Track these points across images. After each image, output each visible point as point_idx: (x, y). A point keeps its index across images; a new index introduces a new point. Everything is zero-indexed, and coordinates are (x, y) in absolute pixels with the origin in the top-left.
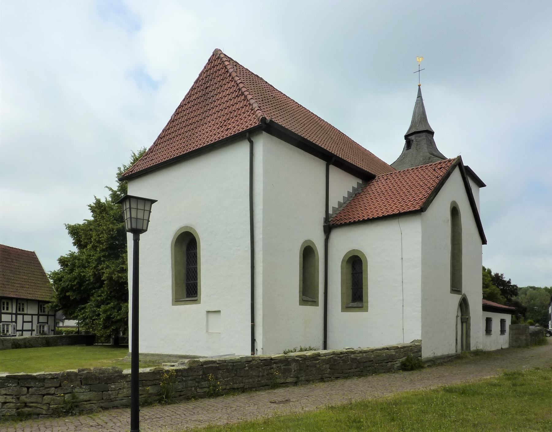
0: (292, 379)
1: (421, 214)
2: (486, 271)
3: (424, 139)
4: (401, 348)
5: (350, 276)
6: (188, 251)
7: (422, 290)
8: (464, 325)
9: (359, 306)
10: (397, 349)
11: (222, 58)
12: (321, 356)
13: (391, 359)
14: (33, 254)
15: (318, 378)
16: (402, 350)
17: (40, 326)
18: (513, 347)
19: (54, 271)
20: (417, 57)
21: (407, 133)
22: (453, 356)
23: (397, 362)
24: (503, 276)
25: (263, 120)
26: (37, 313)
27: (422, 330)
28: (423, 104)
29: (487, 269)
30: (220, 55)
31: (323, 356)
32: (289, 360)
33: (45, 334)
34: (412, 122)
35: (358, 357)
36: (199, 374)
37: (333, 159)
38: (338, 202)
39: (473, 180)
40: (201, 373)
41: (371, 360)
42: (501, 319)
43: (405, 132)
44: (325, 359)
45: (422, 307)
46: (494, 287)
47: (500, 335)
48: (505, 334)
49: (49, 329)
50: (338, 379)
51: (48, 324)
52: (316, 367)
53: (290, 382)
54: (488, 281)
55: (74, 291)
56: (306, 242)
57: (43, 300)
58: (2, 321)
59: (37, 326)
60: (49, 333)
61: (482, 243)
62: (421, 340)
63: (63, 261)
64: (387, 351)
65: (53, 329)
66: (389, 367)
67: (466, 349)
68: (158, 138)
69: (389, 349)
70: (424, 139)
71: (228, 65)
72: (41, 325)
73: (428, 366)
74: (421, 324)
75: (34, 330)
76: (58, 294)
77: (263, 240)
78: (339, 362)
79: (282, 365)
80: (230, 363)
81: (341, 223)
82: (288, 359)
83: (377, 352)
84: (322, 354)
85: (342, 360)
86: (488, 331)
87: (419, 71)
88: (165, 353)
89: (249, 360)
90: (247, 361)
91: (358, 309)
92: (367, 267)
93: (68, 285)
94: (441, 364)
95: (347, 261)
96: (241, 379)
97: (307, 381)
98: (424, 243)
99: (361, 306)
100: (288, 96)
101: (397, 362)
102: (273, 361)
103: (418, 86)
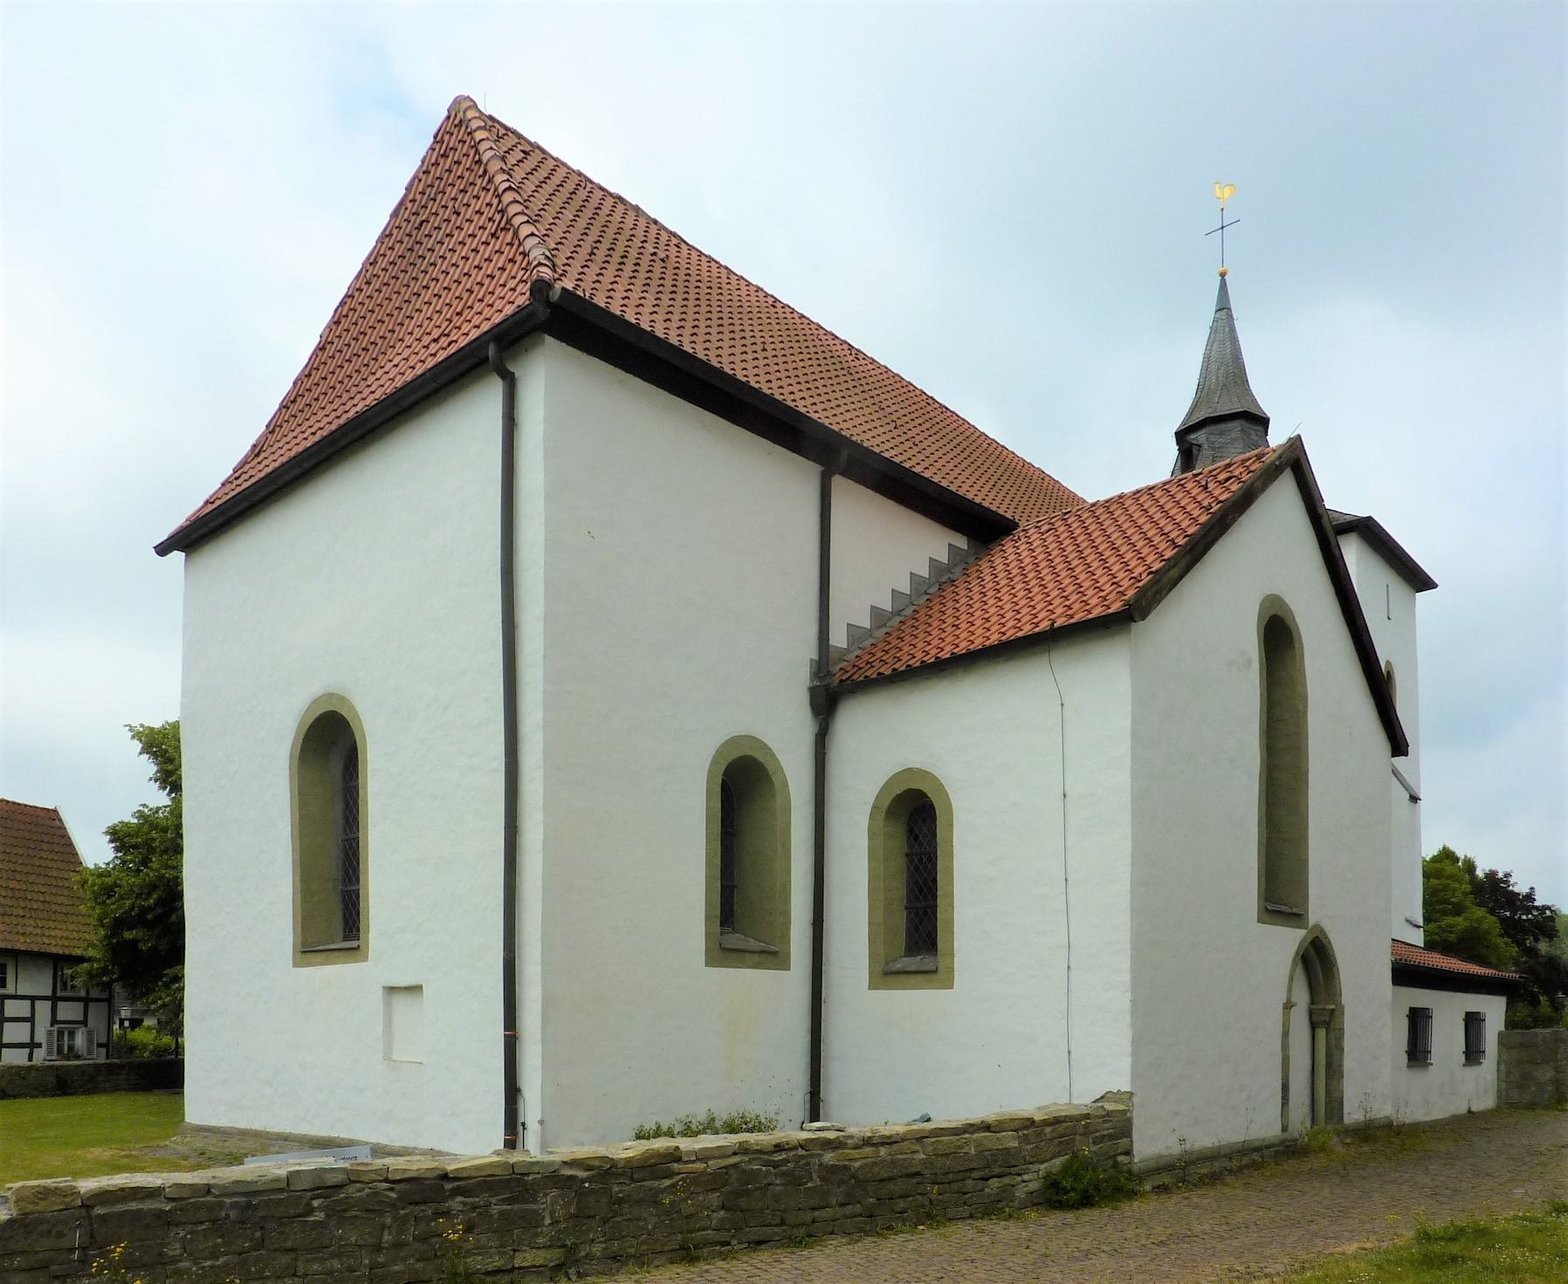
0: (542, 1253)
1: (1130, 630)
2: (1460, 864)
3: (1237, 439)
4: (1046, 1123)
5: (899, 863)
6: (348, 783)
7: (1132, 910)
8: (1321, 1033)
9: (926, 968)
10: (1026, 1128)
11: (470, 120)
12: (686, 1159)
13: (1001, 1164)
14: (53, 815)
15: (666, 1248)
16: (1048, 1129)
17: (60, 1033)
18: (1511, 1105)
19: (95, 865)
20: (1216, 183)
21: (1184, 423)
22: (1267, 1147)
23: (1026, 1177)
24: (1510, 879)
25: (540, 289)
26: (49, 993)
27: (1134, 1054)
28: (1233, 330)
29: (1463, 857)
30: (465, 112)
31: (693, 1162)
32: (531, 1178)
33: (78, 1057)
34: (1200, 389)
35: (855, 1160)
36: (64, 1243)
37: (844, 454)
38: (873, 607)
39: (1393, 568)
40: (77, 1238)
41: (914, 1170)
42: (1467, 1013)
43: (1176, 421)
44: (703, 1173)
45: (1133, 970)
46: (1480, 912)
47: (1464, 1065)
48: (1481, 1063)
49: (90, 1041)
50: (763, 1247)
51: (86, 1026)
52: (656, 1203)
53: (535, 1266)
54: (1463, 893)
55: (149, 925)
56: (733, 741)
57: (67, 952)
58: (6, 1015)
59: (50, 1033)
60: (90, 1052)
61: (1390, 753)
62: (1131, 1094)
63: (119, 836)
64: (986, 1137)
65: (104, 1040)
66: (989, 1195)
67: (1328, 1119)
68: (280, 409)
69: (993, 1129)
70: (1237, 439)
71: (483, 140)
72: (62, 1030)
73: (1159, 1187)
74: (1129, 1033)
75: (39, 1046)
76: (106, 936)
77: (544, 728)
78: (765, 1182)
79: (493, 1200)
80: (236, 1194)
81: (866, 677)
82: (528, 1174)
83: (641, 1186)
84: (689, 1153)
85: (783, 1174)
86: (1418, 1052)
87: (1223, 227)
88: (275, 1130)
89: (330, 1184)
90: (318, 1188)
91: (920, 978)
92: (952, 829)
93: (132, 907)
94: (1214, 1179)
95: (890, 807)
96: (285, 1259)
97: (614, 1258)
98: (1139, 738)
99: (931, 967)
100: (770, 293)
101: (1026, 1177)
102: (448, 1186)
103: (1218, 275)
